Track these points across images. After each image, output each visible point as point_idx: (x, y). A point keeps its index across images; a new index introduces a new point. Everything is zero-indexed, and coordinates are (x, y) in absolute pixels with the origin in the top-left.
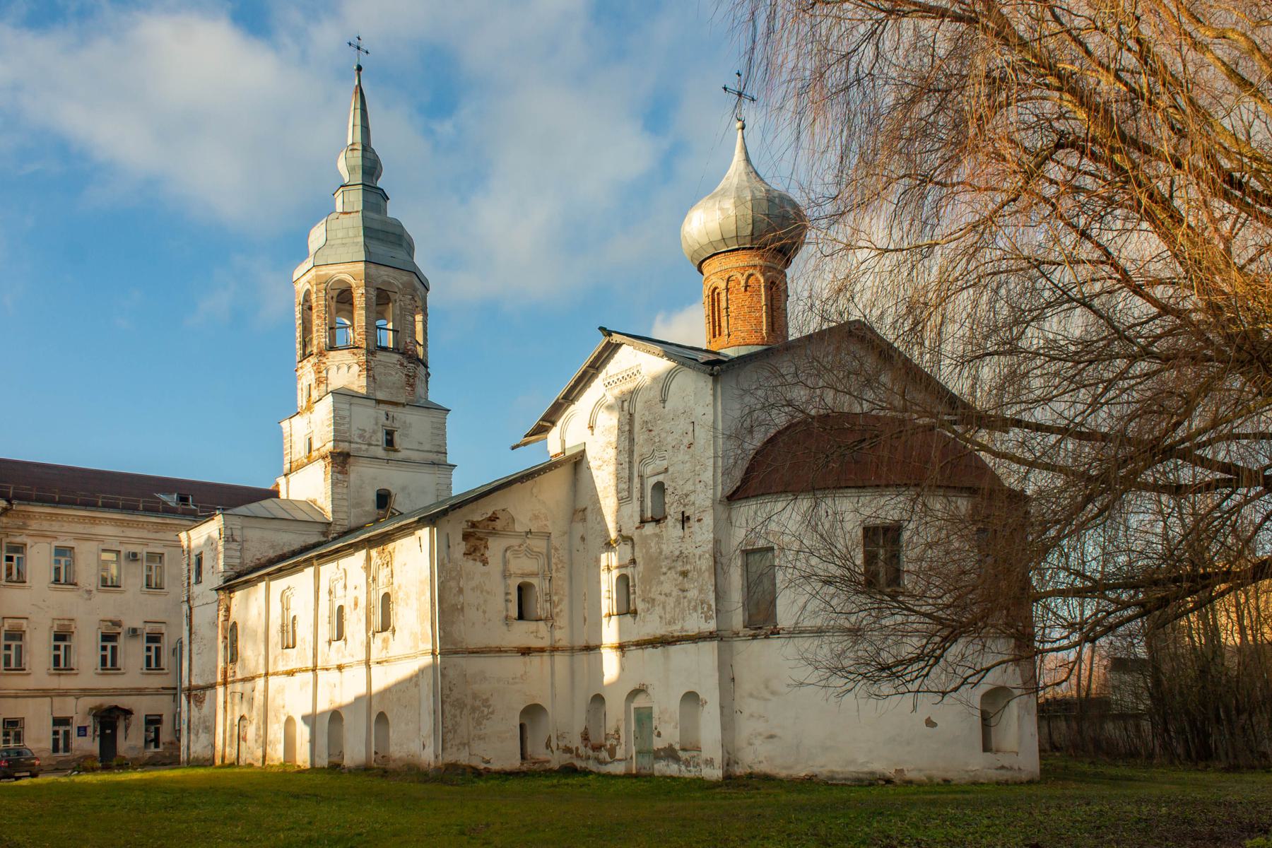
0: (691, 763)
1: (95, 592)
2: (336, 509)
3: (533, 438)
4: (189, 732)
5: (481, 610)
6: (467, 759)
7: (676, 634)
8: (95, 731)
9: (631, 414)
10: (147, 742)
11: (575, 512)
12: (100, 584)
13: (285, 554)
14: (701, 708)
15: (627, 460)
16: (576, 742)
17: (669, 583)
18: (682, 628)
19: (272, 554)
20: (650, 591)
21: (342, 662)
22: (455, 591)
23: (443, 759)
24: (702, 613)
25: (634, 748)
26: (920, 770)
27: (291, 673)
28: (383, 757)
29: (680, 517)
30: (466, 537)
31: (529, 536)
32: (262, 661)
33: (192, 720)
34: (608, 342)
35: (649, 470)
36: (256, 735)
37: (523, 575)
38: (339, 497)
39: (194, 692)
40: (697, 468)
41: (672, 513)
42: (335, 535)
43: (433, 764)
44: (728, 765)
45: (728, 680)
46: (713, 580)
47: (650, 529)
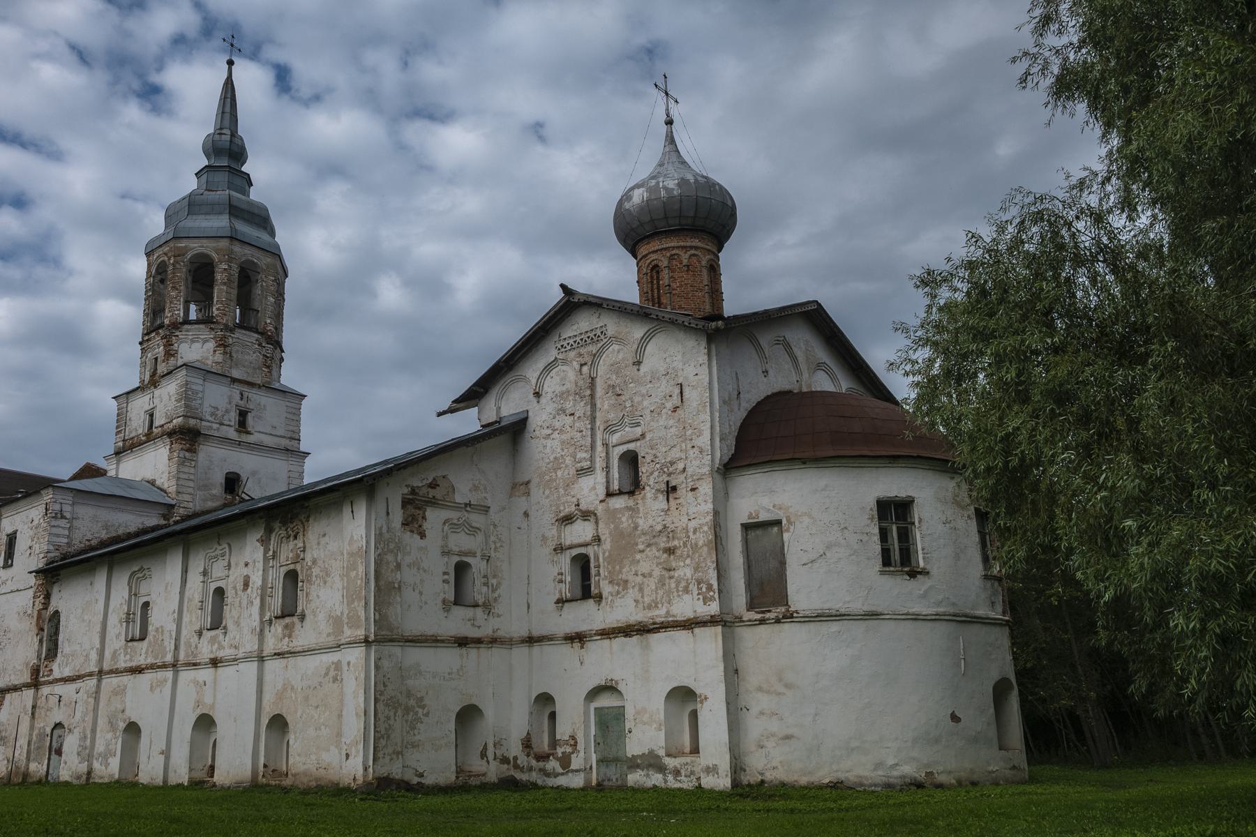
2: (181, 490)
3: (462, 405)
5: (417, 591)
6: (400, 771)
7: (659, 620)
9: (593, 379)
11: (514, 486)
13: (119, 536)
15: (589, 426)
16: (515, 749)
17: (648, 563)
18: (668, 612)
19: (104, 535)
20: (620, 572)
21: (220, 654)
23: (374, 772)
24: (699, 594)
26: (950, 772)
27: (138, 670)
28: (273, 771)
29: (663, 487)
30: (405, 503)
31: (468, 509)
32: (94, 656)
34: (568, 301)
35: (615, 438)
37: (460, 554)
40: (689, 433)
41: (651, 483)
42: (178, 518)
43: (360, 780)
44: (735, 772)
45: (733, 673)
46: (714, 556)
47: (619, 503)
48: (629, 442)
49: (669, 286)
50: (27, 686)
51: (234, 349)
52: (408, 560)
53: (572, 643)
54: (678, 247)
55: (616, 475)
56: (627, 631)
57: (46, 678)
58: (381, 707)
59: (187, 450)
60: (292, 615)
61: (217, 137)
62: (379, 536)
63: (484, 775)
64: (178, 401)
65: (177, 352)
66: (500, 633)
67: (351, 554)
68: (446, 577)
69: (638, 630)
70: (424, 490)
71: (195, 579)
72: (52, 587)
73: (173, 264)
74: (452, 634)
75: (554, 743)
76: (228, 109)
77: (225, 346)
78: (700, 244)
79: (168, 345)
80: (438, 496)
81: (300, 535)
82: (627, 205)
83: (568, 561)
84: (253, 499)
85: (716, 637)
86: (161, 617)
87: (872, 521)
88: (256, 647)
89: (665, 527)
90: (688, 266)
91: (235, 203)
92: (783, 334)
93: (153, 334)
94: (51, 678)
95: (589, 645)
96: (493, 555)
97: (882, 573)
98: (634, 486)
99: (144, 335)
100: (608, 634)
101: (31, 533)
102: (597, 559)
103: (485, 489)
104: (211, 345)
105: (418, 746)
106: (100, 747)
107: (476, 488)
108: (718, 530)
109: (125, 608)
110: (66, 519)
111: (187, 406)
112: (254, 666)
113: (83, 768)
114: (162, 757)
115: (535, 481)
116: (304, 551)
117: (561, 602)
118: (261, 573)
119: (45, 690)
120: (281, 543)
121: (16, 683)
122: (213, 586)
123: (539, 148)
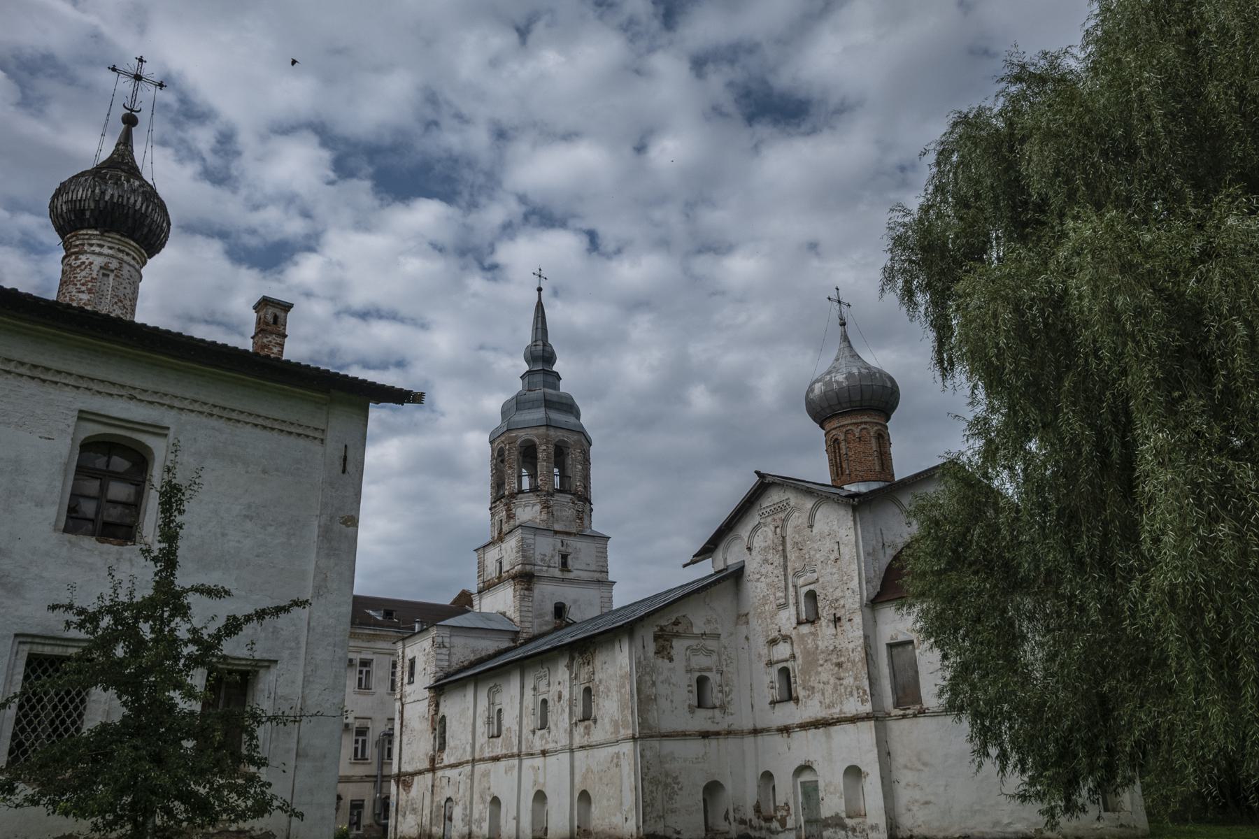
0: (857, 829)
3: (700, 558)
4: (397, 814)
6: (662, 830)
7: (835, 716)
10: (351, 824)
11: (739, 617)
13: (482, 658)
14: (863, 780)
16: (750, 814)
17: (826, 673)
18: (841, 710)
19: (472, 658)
20: (809, 681)
21: (547, 747)
22: (649, 683)
25: (802, 818)
27: (496, 759)
28: (584, 830)
29: (832, 618)
30: (657, 638)
32: (469, 748)
33: (400, 803)
34: (762, 482)
37: (700, 670)
38: (526, 609)
39: (403, 778)
40: (845, 578)
41: (825, 614)
44: (891, 829)
45: (885, 755)
47: (805, 629)
48: (810, 584)
49: (846, 454)
50: (428, 770)
51: (555, 508)
52: (661, 678)
54: (851, 424)
55: (804, 609)
57: (439, 765)
58: (646, 784)
59: (526, 589)
60: (589, 719)
61: (533, 348)
62: (639, 663)
63: (728, 833)
64: (517, 552)
65: (515, 515)
66: (734, 727)
67: (621, 677)
68: (690, 688)
69: (823, 724)
70: (670, 627)
71: (529, 693)
73: (508, 450)
74: (697, 729)
76: (540, 325)
77: (548, 508)
78: (868, 420)
79: (509, 510)
80: (680, 631)
81: (591, 663)
82: (811, 396)
83: (776, 672)
84: (575, 622)
85: (871, 729)
86: (509, 720)
89: (835, 647)
90: (860, 438)
91: (547, 398)
93: (498, 503)
94: (442, 765)
95: (794, 735)
96: (725, 669)
98: (813, 619)
99: (492, 503)
100: (804, 726)
101: (425, 658)
103: (716, 621)
104: (538, 507)
105: (675, 812)
106: (476, 815)
107: (709, 622)
108: (868, 649)
109: (487, 713)
111: (523, 556)
112: (567, 755)
113: (466, 830)
114: (515, 821)
115: (752, 613)
116: (593, 674)
117: (773, 703)
118: (568, 689)
119: (439, 774)
121: (421, 768)
122: (540, 698)
123: (815, 262)
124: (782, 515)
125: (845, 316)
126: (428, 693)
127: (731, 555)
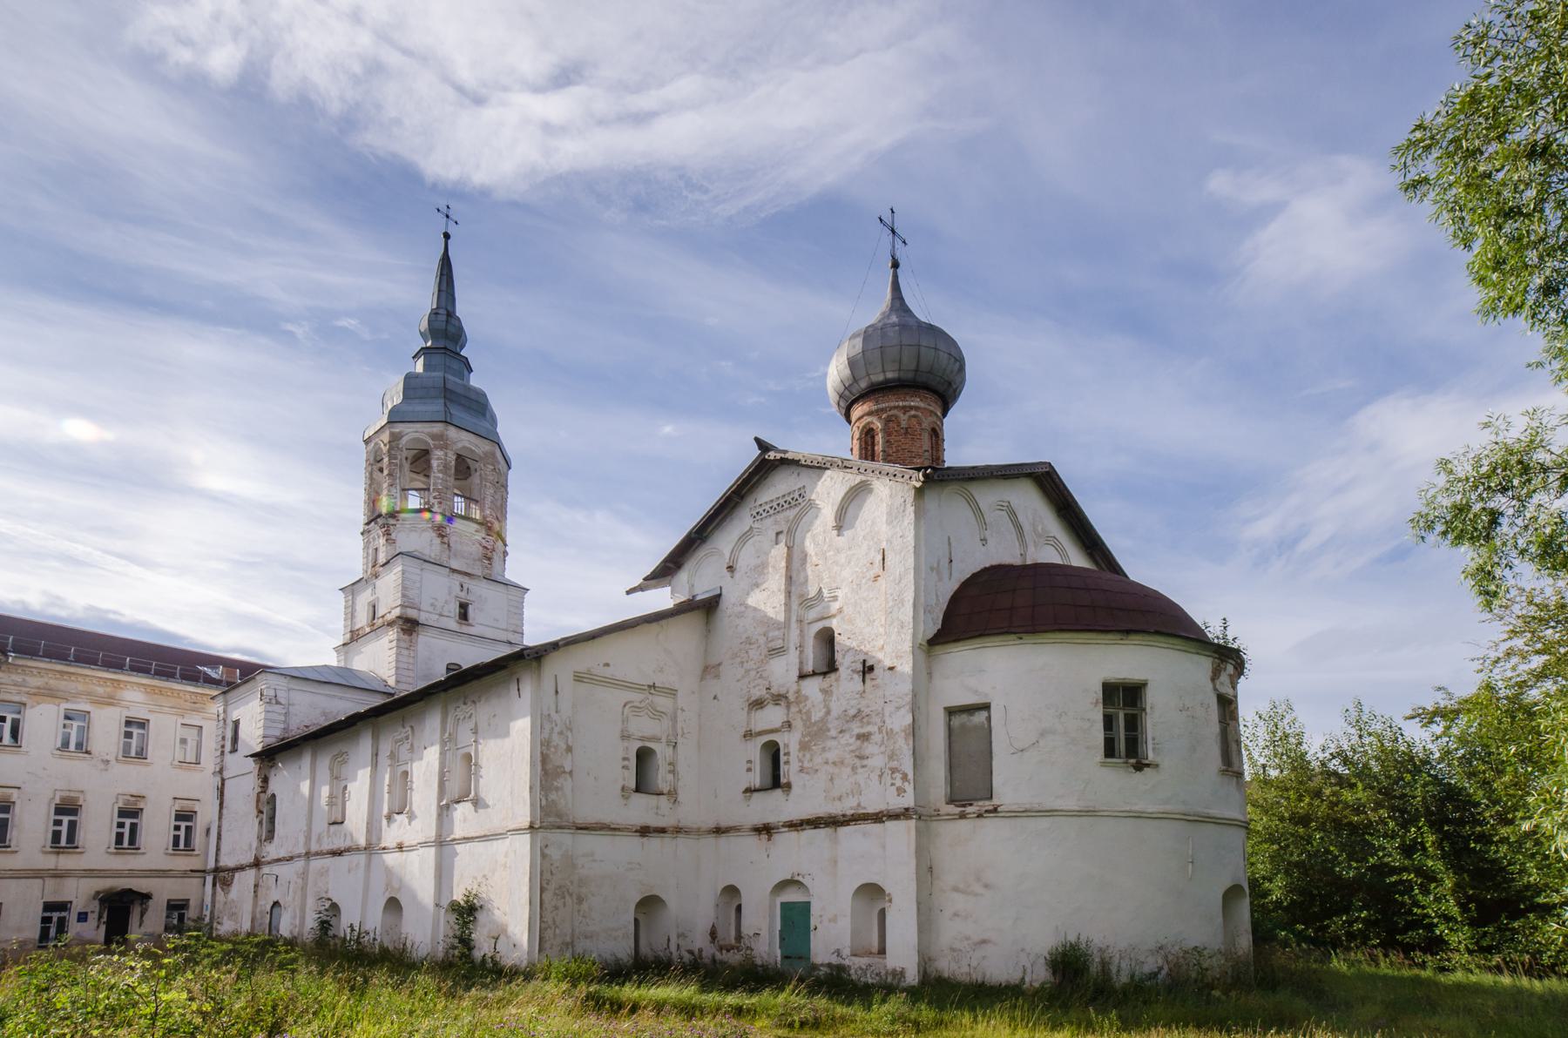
1: (113, 762)
8: (100, 917)
12: (121, 753)
29: (860, 667)
31: (652, 691)
32: (302, 839)
36: (292, 924)
37: (642, 739)
45: (927, 871)
46: (911, 742)
47: (813, 687)
50: (251, 866)
53: (760, 834)
54: (896, 407)
56: (815, 823)
68: (626, 763)
72: (269, 772)
75: (739, 937)
78: (922, 405)
87: (1096, 706)
88: (433, 833)
91: (449, 386)
92: (1008, 499)
95: (776, 837)
97: (1103, 764)
102: (786, 746)
110: (281, 704)
111: (404, 596)
117: (749, 791)
119: (266, 870)
120: (457, 725)
124: (791, 513)
125: (898, 255)
126: (253, 764)
127: (699, 579)
